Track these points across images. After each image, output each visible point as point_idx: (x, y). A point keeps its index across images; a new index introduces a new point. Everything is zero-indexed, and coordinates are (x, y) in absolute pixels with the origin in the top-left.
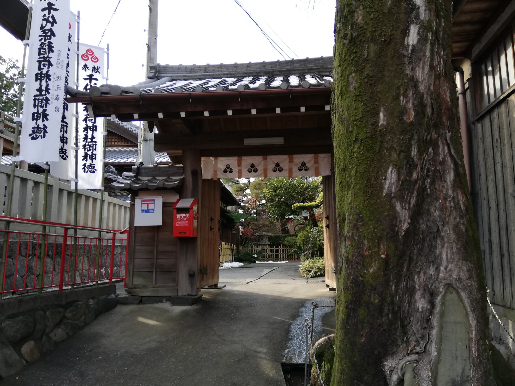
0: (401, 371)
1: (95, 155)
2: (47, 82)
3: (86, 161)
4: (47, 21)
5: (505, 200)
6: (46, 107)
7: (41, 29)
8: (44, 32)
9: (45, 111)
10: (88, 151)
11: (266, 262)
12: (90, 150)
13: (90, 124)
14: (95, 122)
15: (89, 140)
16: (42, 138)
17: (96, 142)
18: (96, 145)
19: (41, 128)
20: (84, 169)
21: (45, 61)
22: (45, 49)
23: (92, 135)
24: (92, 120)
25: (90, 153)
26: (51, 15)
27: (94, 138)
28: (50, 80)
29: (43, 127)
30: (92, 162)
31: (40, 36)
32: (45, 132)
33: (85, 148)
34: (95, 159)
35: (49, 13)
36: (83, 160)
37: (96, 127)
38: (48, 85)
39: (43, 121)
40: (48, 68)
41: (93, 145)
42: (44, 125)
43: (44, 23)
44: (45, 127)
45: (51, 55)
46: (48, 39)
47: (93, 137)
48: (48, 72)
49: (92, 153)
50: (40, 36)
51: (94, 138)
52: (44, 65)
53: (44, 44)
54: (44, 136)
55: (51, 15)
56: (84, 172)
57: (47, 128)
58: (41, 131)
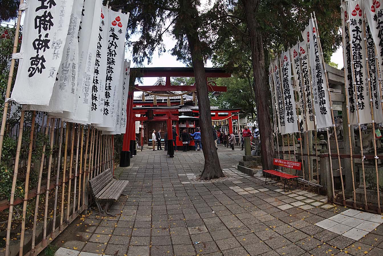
0: (57, 215)
1: (293, 112)
2: (360, 77)
3: (289, 116)
4: (356, 38)
5: (20, 73)
6: (362, 92)
7: (108, 48)
8: (110, 50)
9: (361, 94)
10: (289, 110)
11: (340, 164)
12: (289, 110)
13: (287, 95)
14: (289, 93)
15: (288, 104)
16: (361, 109)
17: (291, 104)
18: (292, 106)
19: (360, 104)
20: (288, 120)
21: (357, 63)
22: (357, 56)
23: (289, 101)
24: (287, 92)
25: (290, 111)
26: (358, 35)
27: (291, 102)
28: (362, 76)
29: (361, 103)
30: (292, 116)
31: (108, 53)
32: (363, 106)
33: (287, 109)
34: (293, 114)
35: (357, 34)
36: (287, 116)
37: (290, 96)
38: (361, 79)
39: (361, 100)
40: (360, 68)
41: (291, 106)
42: (362, 102)
43: (354, 39)
44: (363, 103)
45: (361, 61)
46: (358, 50)
47: (290, 102)
48: (360, 70)
49: (291, 111)
50: (108, 53)
51: (291, 102)
52: (356, 66)
53: (356, 53)
54: (363, 108)
55: (358, 35)
56: (289, 122)
57: (364, 103)
58: (361, 106)
